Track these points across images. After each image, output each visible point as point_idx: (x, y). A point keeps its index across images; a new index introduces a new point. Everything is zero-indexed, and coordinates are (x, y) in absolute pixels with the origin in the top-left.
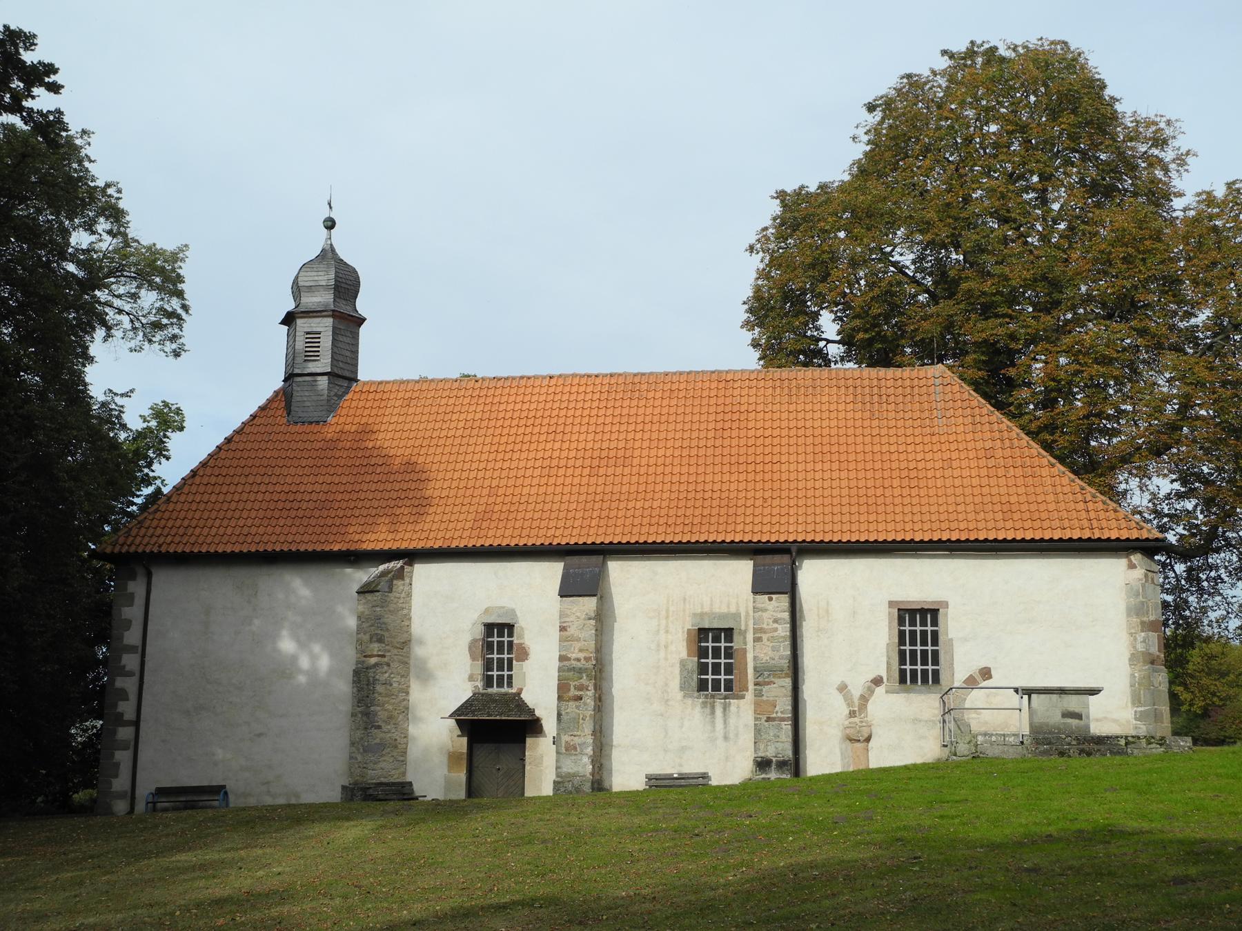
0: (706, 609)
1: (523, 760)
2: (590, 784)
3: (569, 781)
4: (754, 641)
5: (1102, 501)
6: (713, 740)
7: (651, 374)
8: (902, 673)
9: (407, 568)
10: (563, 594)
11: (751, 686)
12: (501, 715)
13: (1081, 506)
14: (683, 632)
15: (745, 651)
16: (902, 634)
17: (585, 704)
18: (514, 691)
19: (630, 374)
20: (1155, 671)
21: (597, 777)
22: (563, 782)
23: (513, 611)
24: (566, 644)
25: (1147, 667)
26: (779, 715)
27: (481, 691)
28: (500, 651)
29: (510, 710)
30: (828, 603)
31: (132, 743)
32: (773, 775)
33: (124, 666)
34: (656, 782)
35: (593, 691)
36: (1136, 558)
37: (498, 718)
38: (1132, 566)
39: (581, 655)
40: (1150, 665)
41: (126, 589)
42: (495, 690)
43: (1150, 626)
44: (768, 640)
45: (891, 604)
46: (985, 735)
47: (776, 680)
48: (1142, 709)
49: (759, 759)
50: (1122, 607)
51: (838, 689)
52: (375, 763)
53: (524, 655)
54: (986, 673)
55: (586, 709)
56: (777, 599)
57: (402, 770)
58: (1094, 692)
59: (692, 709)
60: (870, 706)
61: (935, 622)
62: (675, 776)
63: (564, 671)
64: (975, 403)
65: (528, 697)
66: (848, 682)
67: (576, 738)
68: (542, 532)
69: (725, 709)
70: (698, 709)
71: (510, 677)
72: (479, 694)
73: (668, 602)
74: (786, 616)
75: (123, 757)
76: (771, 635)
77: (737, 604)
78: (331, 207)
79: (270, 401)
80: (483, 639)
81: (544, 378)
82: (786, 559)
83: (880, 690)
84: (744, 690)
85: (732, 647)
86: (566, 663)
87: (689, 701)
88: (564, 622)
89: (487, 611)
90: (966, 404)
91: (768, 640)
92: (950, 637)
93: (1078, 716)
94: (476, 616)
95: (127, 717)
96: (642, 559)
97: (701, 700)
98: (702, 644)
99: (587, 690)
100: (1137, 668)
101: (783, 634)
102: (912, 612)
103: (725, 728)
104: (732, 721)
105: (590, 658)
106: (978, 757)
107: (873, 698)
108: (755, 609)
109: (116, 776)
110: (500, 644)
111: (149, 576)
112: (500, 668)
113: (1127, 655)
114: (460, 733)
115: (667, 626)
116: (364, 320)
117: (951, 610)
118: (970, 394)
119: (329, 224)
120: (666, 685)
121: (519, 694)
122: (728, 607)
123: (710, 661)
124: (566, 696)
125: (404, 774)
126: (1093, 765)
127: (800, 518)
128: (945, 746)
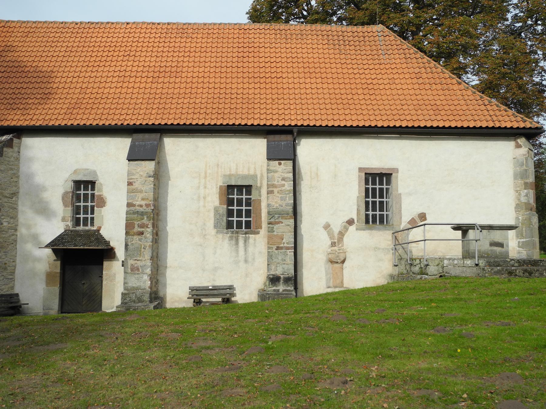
0: (233, 172)
1: (101, 277)
2: (148, 295)
3: (133, 293)
4: (268, 194)
5: (496, 104)
6: (237, 263)
7: (195, 24)
8: (367, 216)
9: (16, 141)
10: (130, 159)
11: (264, 225)
12: (84, 245)
13: (483, 107)
14: (217, 188)
15: (260, 201)
16: (367, 190)
17: (146, 238)
18: (95, 228)
19: (181, 24)
21: (154, 289)
22: (128, 294)
23: (95, 172)
24: (132, 194)
25: (528, 213)
26: (286, 245)
27: (71, 228)
28: (86, 200)
29: (91, 242)
30: (317, 169)
32: (281, 287)
35: (152, 228)
36: (522, 141)
37: (82, 247)
38: (518, 146)
39: (143, 203)
40: (530, 211)
42: (81, 228)
44: (278, 193)
45: (360, 169)
46: (450, 259)
47: (283, 221)
48: (524, 240)
49: (271, 276)
50: (511, 173)
51: (323, 227)
53: (102, 203)
54: (423, 217)
55: (146, 241)
56: (284, 164)
57: (11, 285)
59: (223, 241)
60: (345, 239)
61: (389, 183)
62: (210, 287)
63: (130, 214)
64: (405, 47)
65: (105, 233)
66: (331, 223)
67: (139, 262)
68: (116, 117)
69: (245, 241)
70: (227, 241)
71: (92, 219)
72: (69, 230)
73: (206, 166)
74: (291, 175)
76: (280, 189)
77: (255, 168)
80: (73, 192)
81: (123, 23)
82: (290, 137)
83: (352, 228)
84: (259, 228)
85: (250, 199)
86: (132, 208)
87: (220, 236)
88: (131, 179)
89: (75, 172)
90: (399, 47)
91: (278, 193)
92: (399, 192)
93: (501, 245)
94: (67, 175)
96: (188, 137)
97: (228, 235)
98: (230, 196)
99: (147, 227)
100: (521, 213)
101: (289, 188)
103: (246, 254)
104: (250, 249)
105: (150, 205)
106: (445, 276)
107: (347, 233)
108: (269, 171)
110: (86, 196)
112: (86, 212)
113: (514, 205)
114: (55, 258)
115: (205, 184)
117: (400, 175)
118: (401, 41)
120: (204, 224)
121: (98, 231)
122: (249, 171)
123: (235, 208)
124: (131, 232)
125: (12, 288)
127: (298, 111)
128: (395, 266)
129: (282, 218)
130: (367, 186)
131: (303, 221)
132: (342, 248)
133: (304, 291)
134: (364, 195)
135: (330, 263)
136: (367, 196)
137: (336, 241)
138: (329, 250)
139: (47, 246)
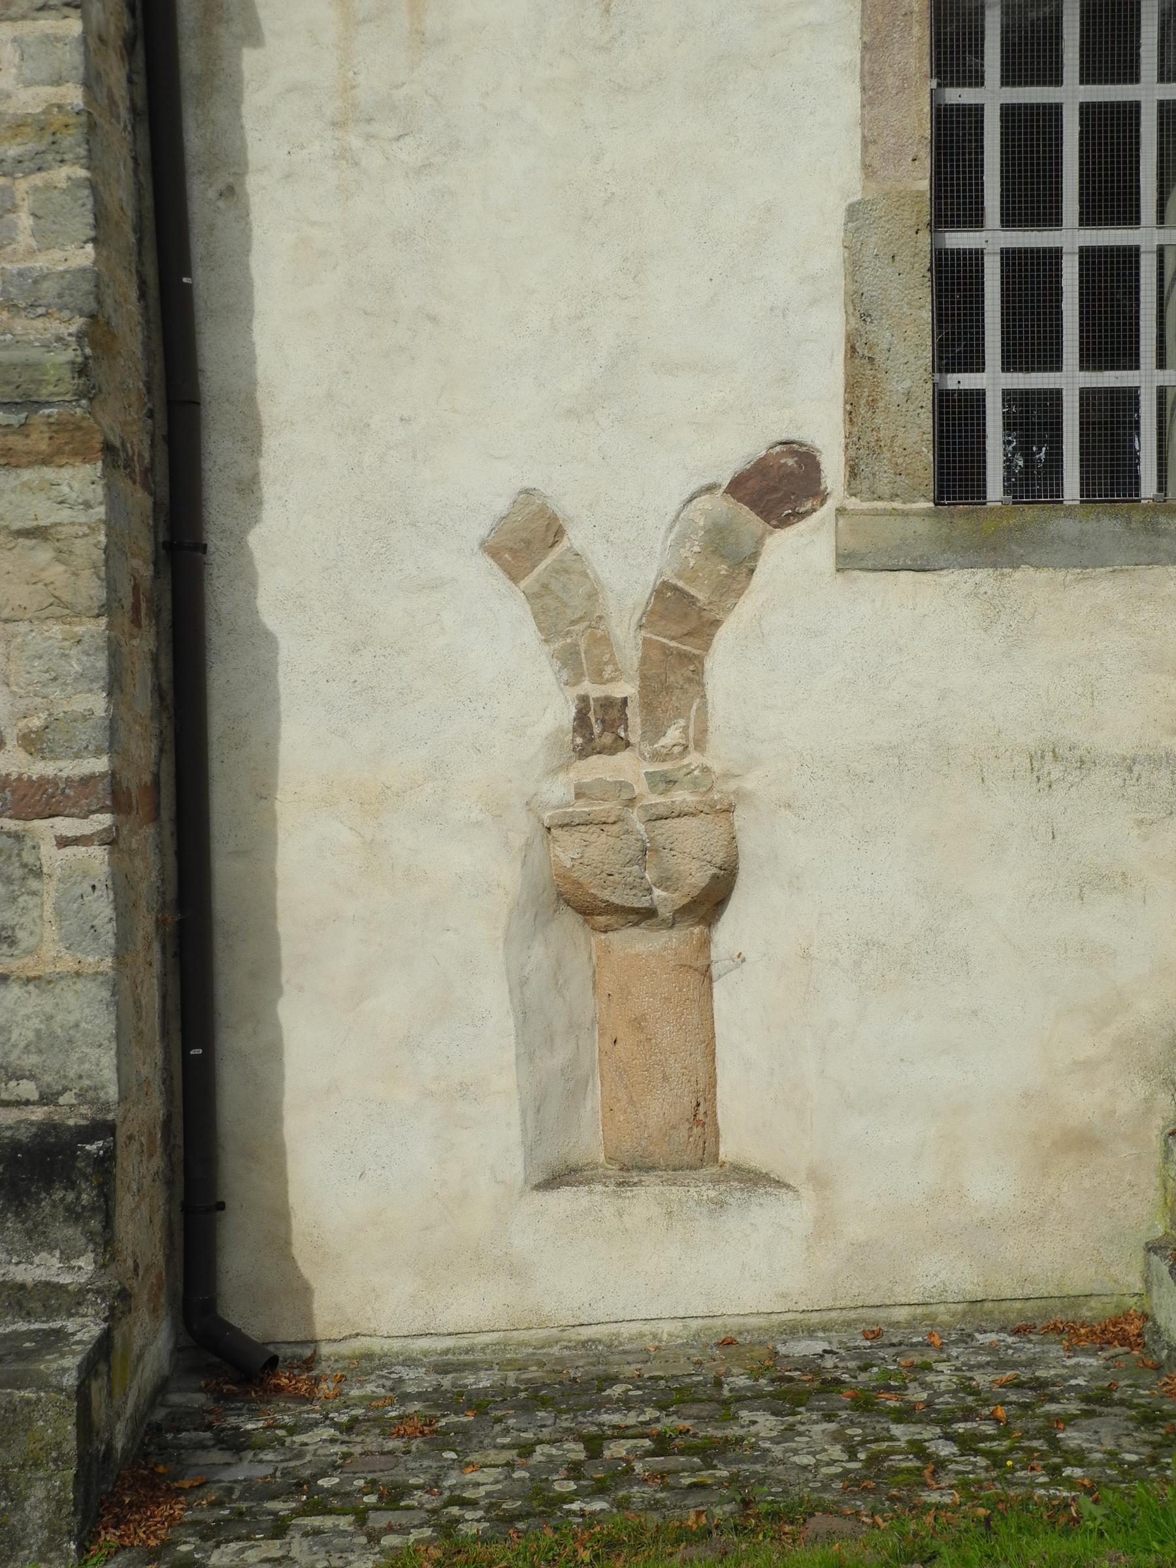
51: (493, 550)
107: (747, 607)
130: (958, 96)
131: (269, 491)
132: (693, 759)
133: (295, 1223)
134: (924, 185)
135: (570, 919)
137: (626, 689)
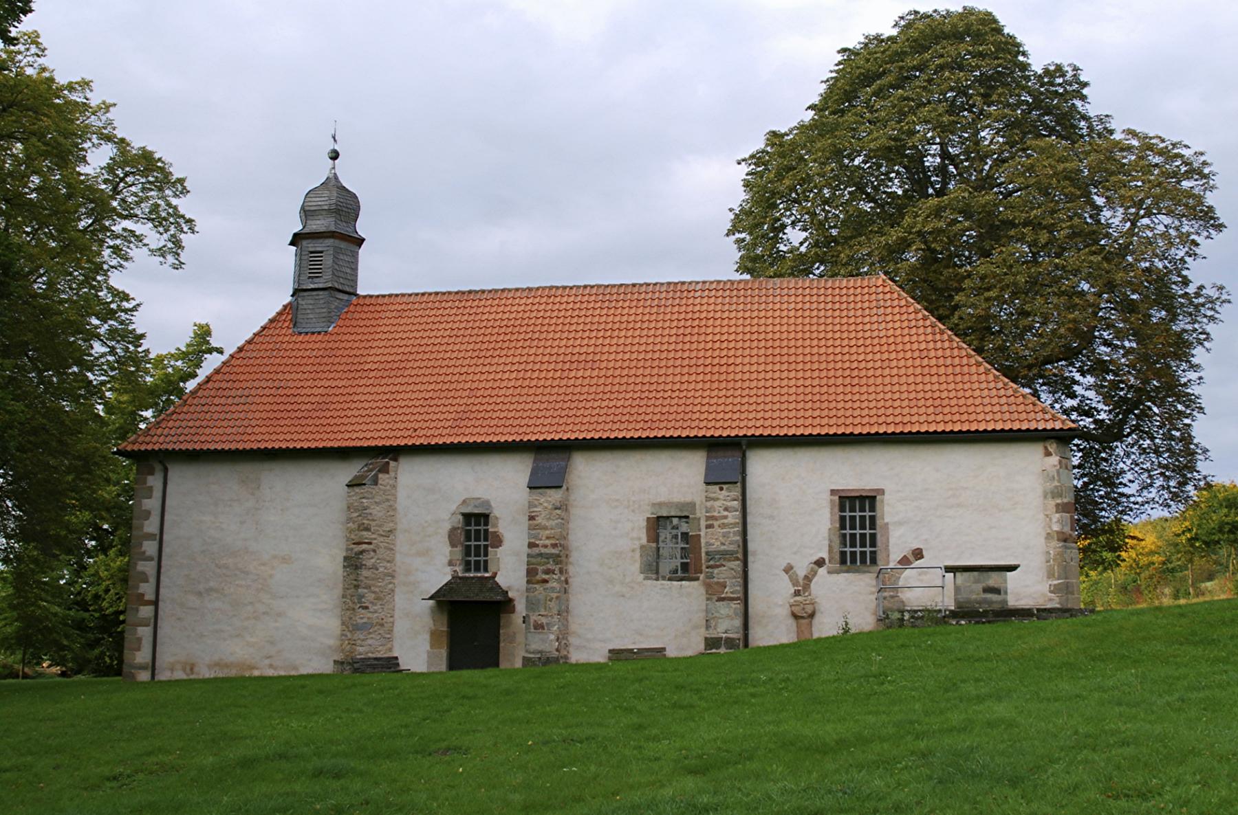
8: (843, 554)
16: (842, 519)
20: (1066, 548)
31: (152, 621)
33: (144, 552)
34: (617, 655)
36: (1052, 447)
38: (1048, 454)
41: (145, 483)
43: (1061, 508)
45: (833, 492)
50: (1039, 491)
52: (363, 640)
53: (498, 541)
57: (389, 646)
58: (1012, 568)
60: (813, 585)
61: (873, 509)
66: (793, 564)
75: (145, 632)
78: (335, 140)
79: (280, 314)
83: (822, 571)
86: (536, 551)
92: (886, 520)
93: (997, 591)
94: (453, 507)
95: (147, 598)
102: (852, 499)
108: (708, 499)
109: (139, 649)
111: (166, 471)
116: (363, 240)
117: (887, 497)
119: (334, 155)
125: (390, 650)
126: (1003, 630)
129: (725, 559)
136: (843, 527)
138: (792, 601)
139: (431, 598)
